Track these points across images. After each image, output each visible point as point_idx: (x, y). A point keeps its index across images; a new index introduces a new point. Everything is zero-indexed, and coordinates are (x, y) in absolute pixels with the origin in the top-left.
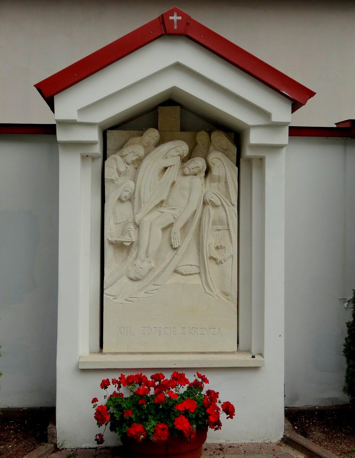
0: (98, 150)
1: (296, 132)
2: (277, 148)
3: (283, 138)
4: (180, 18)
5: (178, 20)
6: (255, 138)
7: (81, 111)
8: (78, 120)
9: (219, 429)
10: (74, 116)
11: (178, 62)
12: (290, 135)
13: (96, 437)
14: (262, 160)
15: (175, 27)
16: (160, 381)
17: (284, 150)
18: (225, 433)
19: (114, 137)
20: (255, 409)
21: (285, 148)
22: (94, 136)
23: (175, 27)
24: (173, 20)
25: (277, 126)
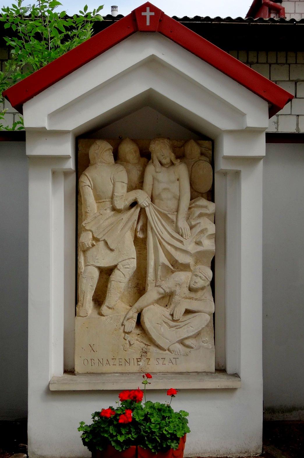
0: (71, 165)
1: (272, 138)
2: (253, 160)
3: (259, 147)
4: (153, 14)
5: (151, 16)
6: (228, 148)
7: (53, 116)
8: (48, 128)
9: (115, 169)
10: (45, 124)
11: (153, 55)
12: (267, 141)
13: (93, 418)
14: (237, 174)
15: (148, 23)
16: (144, 448)
17: (262, 162)
18: (192, 444)
19: (82, 142)
20: (218, 425)
21: (262, 160)
22: (67, 148)
23: (148, 23)
24: (145, 16)
25: (253, 132)
